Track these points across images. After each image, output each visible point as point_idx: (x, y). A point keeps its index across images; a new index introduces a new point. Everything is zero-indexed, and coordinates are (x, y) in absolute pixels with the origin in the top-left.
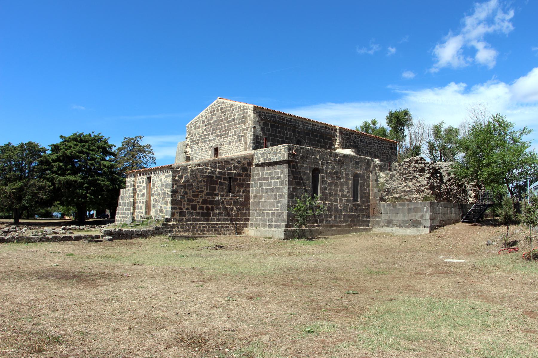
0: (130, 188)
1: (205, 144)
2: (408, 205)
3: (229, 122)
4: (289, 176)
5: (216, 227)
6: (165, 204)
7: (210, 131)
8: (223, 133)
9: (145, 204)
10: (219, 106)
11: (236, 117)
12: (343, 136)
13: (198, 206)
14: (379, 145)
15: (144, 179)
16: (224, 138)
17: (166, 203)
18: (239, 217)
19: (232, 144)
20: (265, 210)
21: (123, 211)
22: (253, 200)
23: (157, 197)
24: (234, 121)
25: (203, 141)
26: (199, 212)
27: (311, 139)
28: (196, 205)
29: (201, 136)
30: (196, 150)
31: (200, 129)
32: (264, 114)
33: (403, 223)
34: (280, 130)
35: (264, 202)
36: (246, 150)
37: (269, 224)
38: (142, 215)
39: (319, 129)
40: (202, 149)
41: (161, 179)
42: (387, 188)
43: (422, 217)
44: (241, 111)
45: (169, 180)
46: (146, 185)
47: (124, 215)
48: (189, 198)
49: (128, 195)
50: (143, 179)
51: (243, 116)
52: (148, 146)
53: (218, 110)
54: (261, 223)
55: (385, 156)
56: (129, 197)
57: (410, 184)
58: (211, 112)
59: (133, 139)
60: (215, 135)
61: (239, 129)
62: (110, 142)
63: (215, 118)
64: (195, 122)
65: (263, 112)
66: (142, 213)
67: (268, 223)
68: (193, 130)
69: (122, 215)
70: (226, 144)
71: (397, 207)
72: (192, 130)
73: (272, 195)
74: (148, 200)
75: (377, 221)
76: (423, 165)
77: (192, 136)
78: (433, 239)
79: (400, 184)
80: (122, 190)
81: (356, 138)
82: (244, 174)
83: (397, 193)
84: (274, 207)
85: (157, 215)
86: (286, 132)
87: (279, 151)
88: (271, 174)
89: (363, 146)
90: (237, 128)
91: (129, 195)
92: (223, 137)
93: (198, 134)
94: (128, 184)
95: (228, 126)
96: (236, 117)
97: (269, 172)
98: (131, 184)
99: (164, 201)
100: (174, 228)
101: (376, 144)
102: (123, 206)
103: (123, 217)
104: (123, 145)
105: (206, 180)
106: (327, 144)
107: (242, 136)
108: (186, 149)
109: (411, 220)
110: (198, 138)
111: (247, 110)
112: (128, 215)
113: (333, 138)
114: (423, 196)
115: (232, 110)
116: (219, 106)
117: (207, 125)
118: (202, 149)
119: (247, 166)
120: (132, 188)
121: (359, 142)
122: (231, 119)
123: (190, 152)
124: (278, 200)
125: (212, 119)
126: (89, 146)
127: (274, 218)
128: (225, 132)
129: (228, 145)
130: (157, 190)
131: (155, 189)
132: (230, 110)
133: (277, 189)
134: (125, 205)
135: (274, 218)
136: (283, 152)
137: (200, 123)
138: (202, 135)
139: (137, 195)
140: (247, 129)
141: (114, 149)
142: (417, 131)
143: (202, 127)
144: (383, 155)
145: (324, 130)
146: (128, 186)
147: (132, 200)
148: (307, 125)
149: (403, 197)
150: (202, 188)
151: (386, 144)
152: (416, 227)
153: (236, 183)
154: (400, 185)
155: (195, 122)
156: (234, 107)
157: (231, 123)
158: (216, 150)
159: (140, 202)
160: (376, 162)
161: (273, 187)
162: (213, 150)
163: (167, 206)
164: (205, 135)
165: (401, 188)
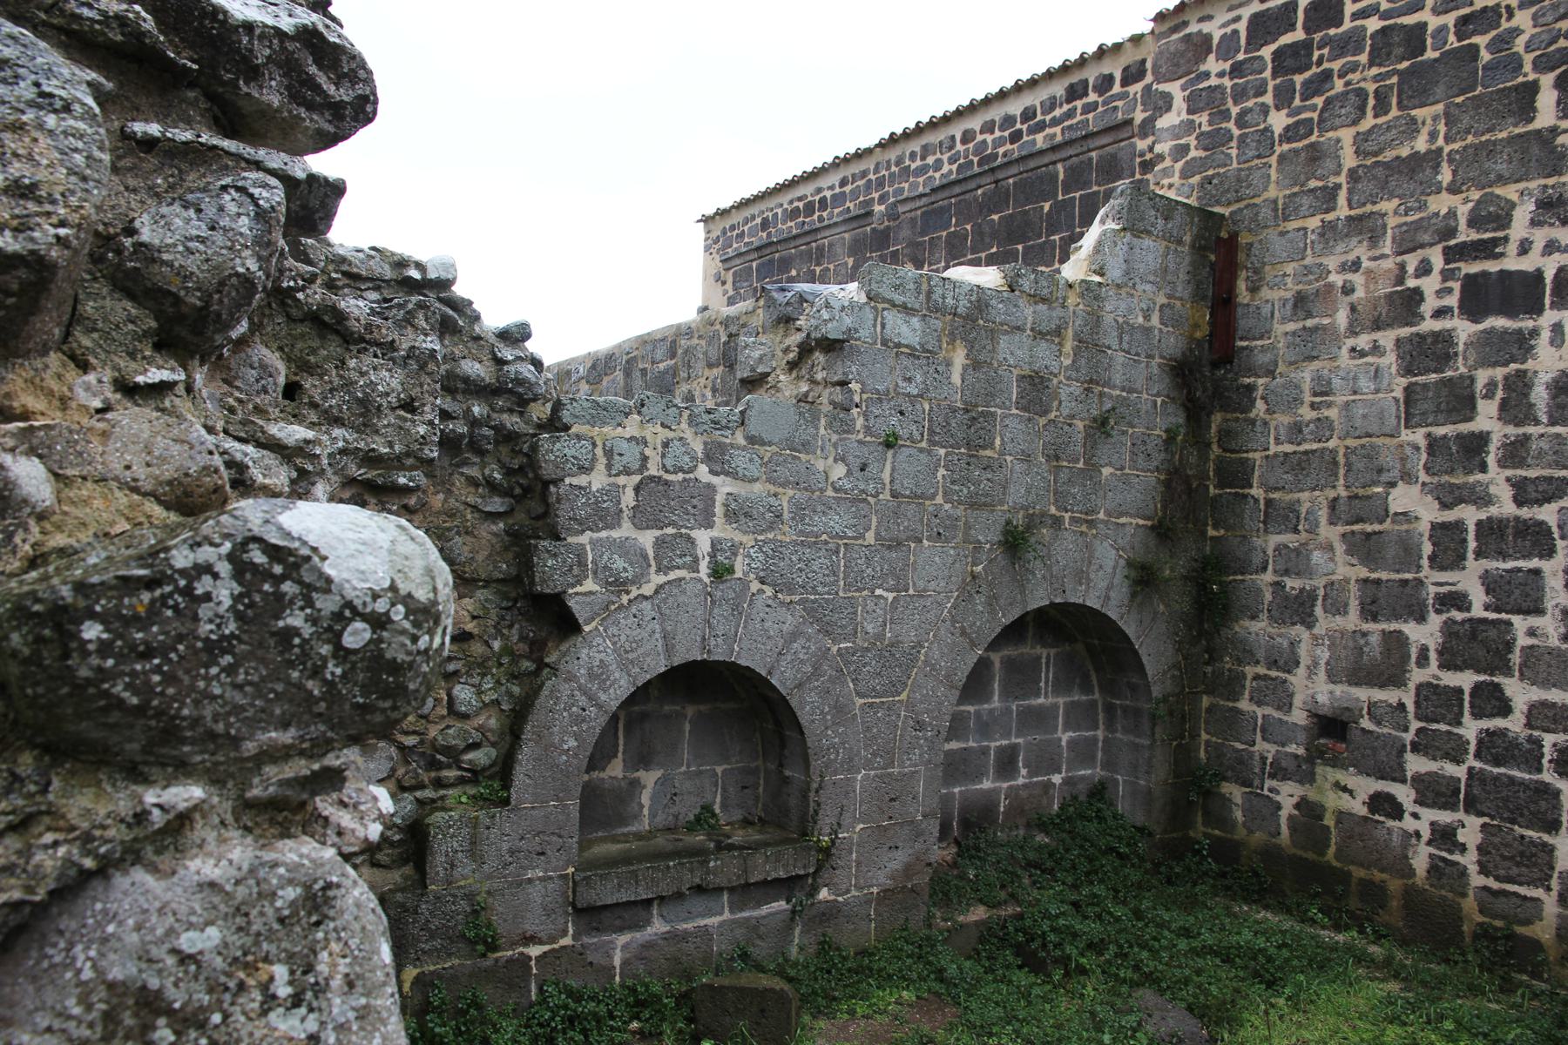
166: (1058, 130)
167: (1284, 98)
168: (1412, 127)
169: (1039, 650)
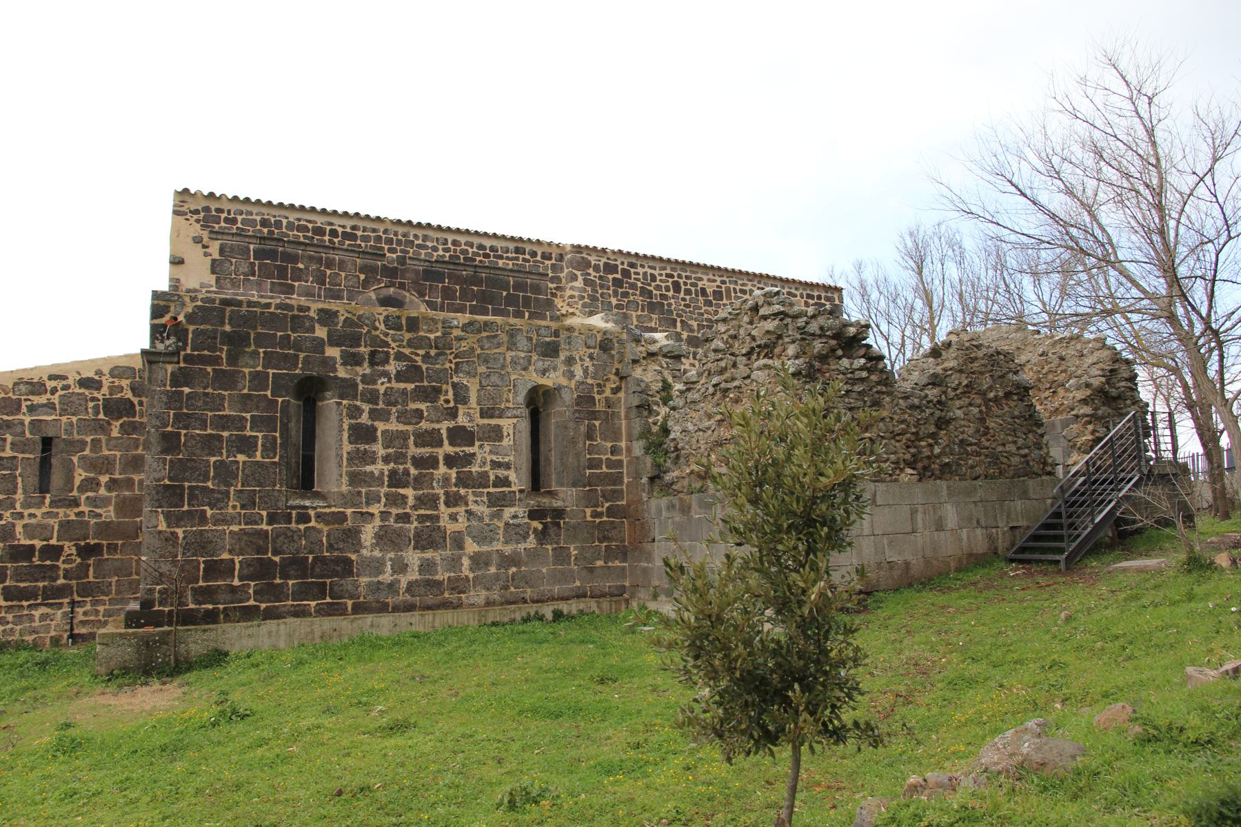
12: (594, 274)
18: (91, 579)
32: (223, 216)
34: (301, 266)
65: (220, 211)
71: (692, 513)
82: (118, 424)
86: (328, 272)
89: (687, 306)
113: (551, 285)
119: (129, 395)
121: (671, 294)
145: (508, 258)
148: (430, 244)
151: (795, 296)
153: (75, 459)
166: (511, 263)
167: (615, 294)
168: (651, 319)
169: (102, 437)
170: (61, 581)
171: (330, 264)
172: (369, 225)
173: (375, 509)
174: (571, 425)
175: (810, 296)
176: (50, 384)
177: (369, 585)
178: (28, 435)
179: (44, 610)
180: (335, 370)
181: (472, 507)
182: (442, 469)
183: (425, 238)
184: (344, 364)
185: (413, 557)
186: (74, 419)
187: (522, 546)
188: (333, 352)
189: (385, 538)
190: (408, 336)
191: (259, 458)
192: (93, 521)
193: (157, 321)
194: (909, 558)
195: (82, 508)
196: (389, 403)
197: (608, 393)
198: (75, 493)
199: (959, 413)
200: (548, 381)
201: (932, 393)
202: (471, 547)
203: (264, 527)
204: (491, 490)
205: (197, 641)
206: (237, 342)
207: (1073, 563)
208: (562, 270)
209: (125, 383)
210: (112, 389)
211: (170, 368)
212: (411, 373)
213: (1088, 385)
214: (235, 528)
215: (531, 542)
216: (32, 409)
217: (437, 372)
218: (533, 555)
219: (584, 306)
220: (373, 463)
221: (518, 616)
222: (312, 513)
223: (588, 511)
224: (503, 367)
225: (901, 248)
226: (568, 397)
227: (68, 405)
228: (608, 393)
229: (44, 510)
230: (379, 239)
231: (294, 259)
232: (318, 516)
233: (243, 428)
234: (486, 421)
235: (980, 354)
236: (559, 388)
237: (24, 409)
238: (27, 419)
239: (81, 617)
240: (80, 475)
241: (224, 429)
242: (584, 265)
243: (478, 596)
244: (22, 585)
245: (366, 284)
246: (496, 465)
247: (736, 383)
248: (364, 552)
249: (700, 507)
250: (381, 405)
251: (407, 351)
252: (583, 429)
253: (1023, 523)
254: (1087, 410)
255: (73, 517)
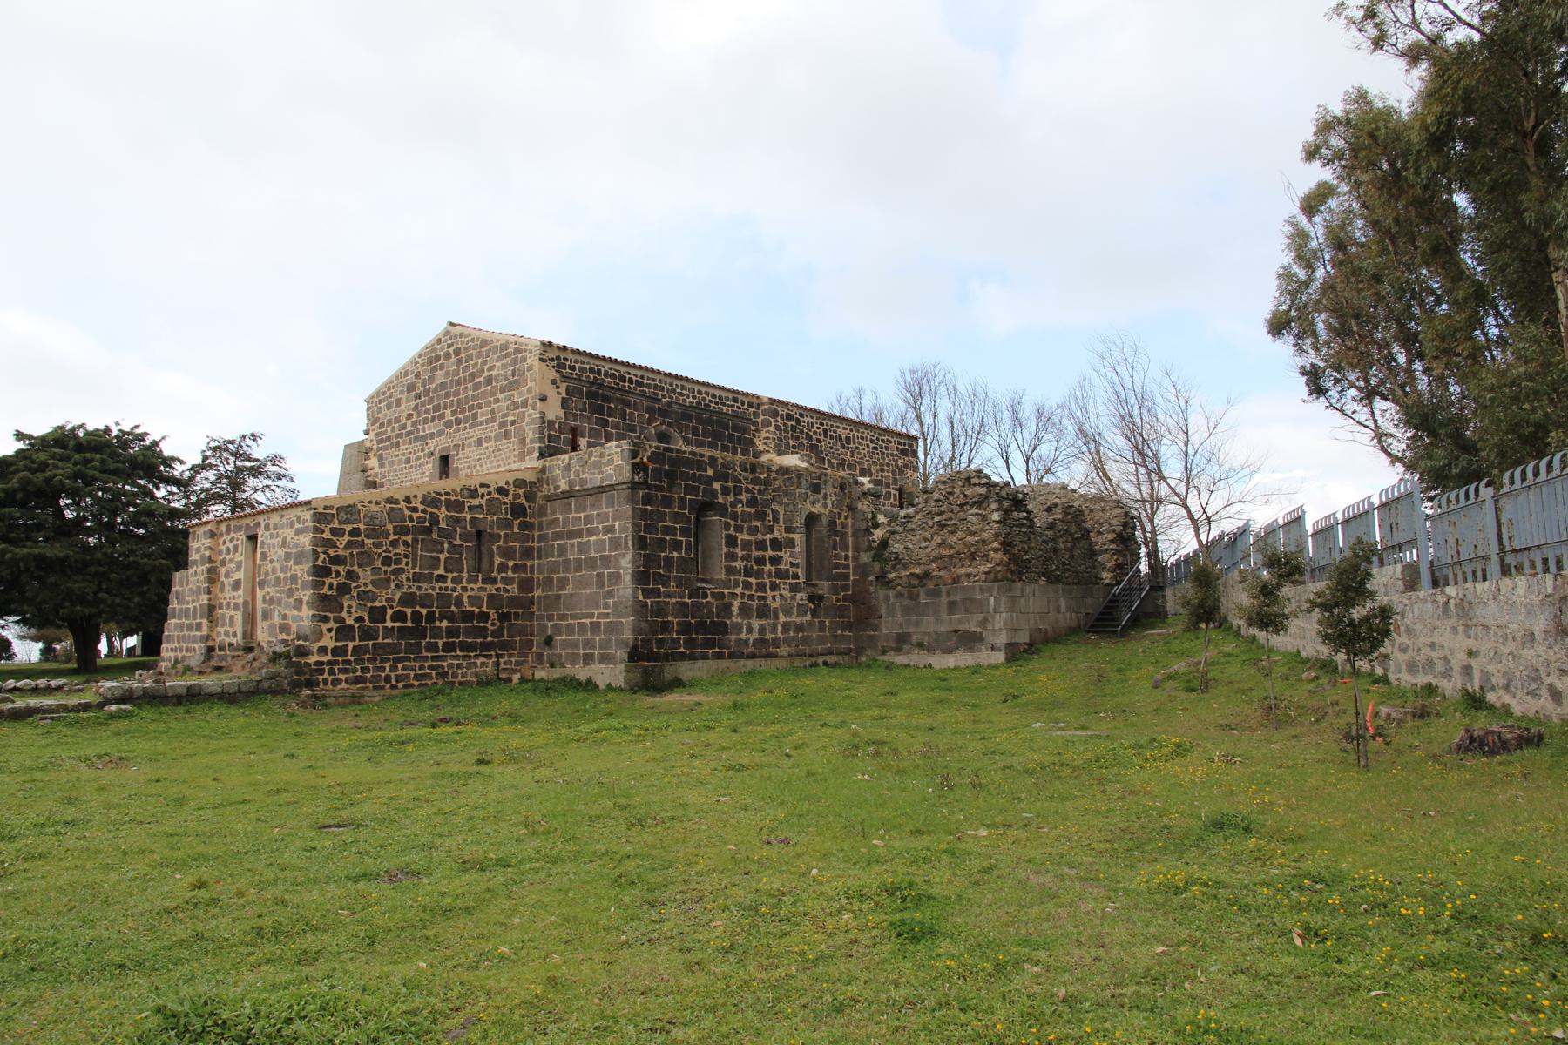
0: (200, 568)
1: (417, 446)
2: (948, 594)
3: (477, 387)
4: (634, 525)
5: (443, 668)
6: (295, 608)
7: (427, 412)
8: (461, 416)
9: (241, 609)
10: (450, 346)
11: (494, 373)
13: (389, 612)
14: (871, 445)
15: (239, 542)
16: (465, 428)
17: (298, 604)
18: (506, 638)
19: (485, 445)
20: (574, 617)
21: (182, 631)
22: (543, 591)
23: (270, 590)
24: (491, 384)
25: (410, 440)
26: (394, 627)
27: (695, 431)
28: (384, 607)
29: (404, 427)
30: (392, 463)
31: (403, 406)
32: (568, 363)
33: (936, 641)
34: (612, 405)
35: (571, 595)
36: (522, 460)
37: (585, 655)
38: (234, 641)
39: (717, 403)
40: (408, 461)
41: (284, 540)
42: (895, 550)
43: (983, 623)
44: (507, 356)
45: (306, 541)
46: (242, 558)
47: (184, 642)
48: (363, 588)
49: (194, 588)
50: (235, 542)
51: (514, 371)
52: (275, 459)
53: (448, 356)
54: (563, 652)
55: (888, 471)
56: (198, 592)
57: (952, 539)
58: (430, 362)
59: (232, 442)
60: (442, 422)
61: (503, 404)
62: (167, 450)
63: (440, 377)
64: (389, 389)
66: (235, 635)
67: (581, 652)
68: (385, 411)
69: (179, 642)
70: (470, 446)
71: (921, 598)
72: (380, 410)
73: (592, 576)
74: (249, 600)
75: (870, 637)
76: (983, 491)
77: (382, 426)
78: (1009, 672)
79: (926, 540)
80: (178, 576)
81: (813, 427)
82: (517, 522)
83: (919, 564)
84: (597, 607)
85: (274, 639)
87: (607, 458)
88: (588, 520)
90: (497, 401)
91: (199, 588)
92: (462, 426)
93: (398, 420)
94: (194, 556)
95: (474, 398)
96: (494, 373)
97: (582, 515)
98: (203, 556)
99: (291, 600)
100: (322, 672)
101: (864, 442)
102: (180, 618)
103: (181, 650)
104: (205, 458)
105: (410, 541)
106: (739, 443)
107: (513, 423)
108: (367, 462)
109: (956, 632)
110: (397, 432)
111: (524, 354)
112: (195, 642)
113: (753, 428)
114: (987, 570)
115: (484, 353)
116: (450, 346)
117: (420, 398)
118: (408, 461)
119: (524, 501)
120: (204, 567)
121: (822, 438)
122: (481, 379)
123: (377, 470)
124: (607, 589)
125: (432, 379)
126: (103, 461)
127: (598, 638)
128: (466, 413)
129: (475, 448)
130: (274, 569)
131: (269, 568)
132: (479, 355)
133: (605, 559)
134: (187, 616)
135: (598, 638)
136: (618, 461)
137: (402, 392)
138: (409, 422)
139: (219, 586)
140: (525, 405)
141: (179, 470)
142: (968, 409)
143: (407, 402)
144: (882, 470)
145: (729, 406)
146: (195, 562)
147: (206, 602)
148: (684, 392)
149: (934, 573)
150: (399, 562)
152: (971, 650)
153: (494, 548)
154: (927, 543)
155: (389, 389)
156: (489, 347)
157: (483, 389)
158: (445, 461)
159: (228, 604)
160: (863, 484)
161: (593, 555)
162: (438, 463)
163: (302, 614)
164: (414, 423)
165: (929, 549)
170: (489, 639)
171: (629, 405)
172: (651, 376)
173: (738, 591)
174: (826, 539)
175: (900, 443)
176: (481, 491)
177: (736, 640)
178: (469, 529)
179: (482, 659)
180: (717, 498)
181: (783, 592)
182: (768, 566)
183: (683, 388)
184: (722, 494)
185: (756, 623)
186: (495, 517)
187: (805, 619)
188: (716, 485)
189: (745, 611)
190: (751, 476)
191: (683, 555)
192: (506, 595)
193: (634, 461)
194: (1048, 627)
195: (499, 585)
196: (744, 521)
197: (842, 519)
198: (495, 574)
199: (1062, 546)
200: (815, 510)
201: (1050, 533)
202: (782, 618)
203: (687, 600)
204: (791, 581)
205: (670, 671)
206: (671, 475)
207: (1124, 633)
208: (758, 416)
209: (521, 491)
210: (516, 496)
211: (641, 492)
212: (752, 502)
213: (1114, 531)
214: (674, 600)
215: (808, 617)
216: (471, 508)
217: (764, 500)
218: (810, 624)
219: (776, 445)
220: (736, 560)
221: (807, 664)
222: (709, 592)
223: (834, 597)
224: (795, 499)
225: (900, 379)
226: (825, 520)
227: (493, 507)
228: (842, 519)
229: (479, 585)
230: (656, 386)
231: (607, 399)
232: (712, 594)
233: (675, 535)
234: (788, 535)
235: (1071, 512)
236: (820, 515)
237: (466, 509)
238: (468, 517)
239: (502, 666)
240: (498, 560)
241: (667, 535)
242: (775, 414)
243: (784, 650)
244: (470, 640)
245: (649, 422)
246: (793, 565)
247: (953, 522)
248: (733, 619)
249: (927, 595)
250: (739, 523)
251: (750, 486)
252: (831, 542)
253: (1091, 611)
254: (1113, 546)
255: (494, 592)
